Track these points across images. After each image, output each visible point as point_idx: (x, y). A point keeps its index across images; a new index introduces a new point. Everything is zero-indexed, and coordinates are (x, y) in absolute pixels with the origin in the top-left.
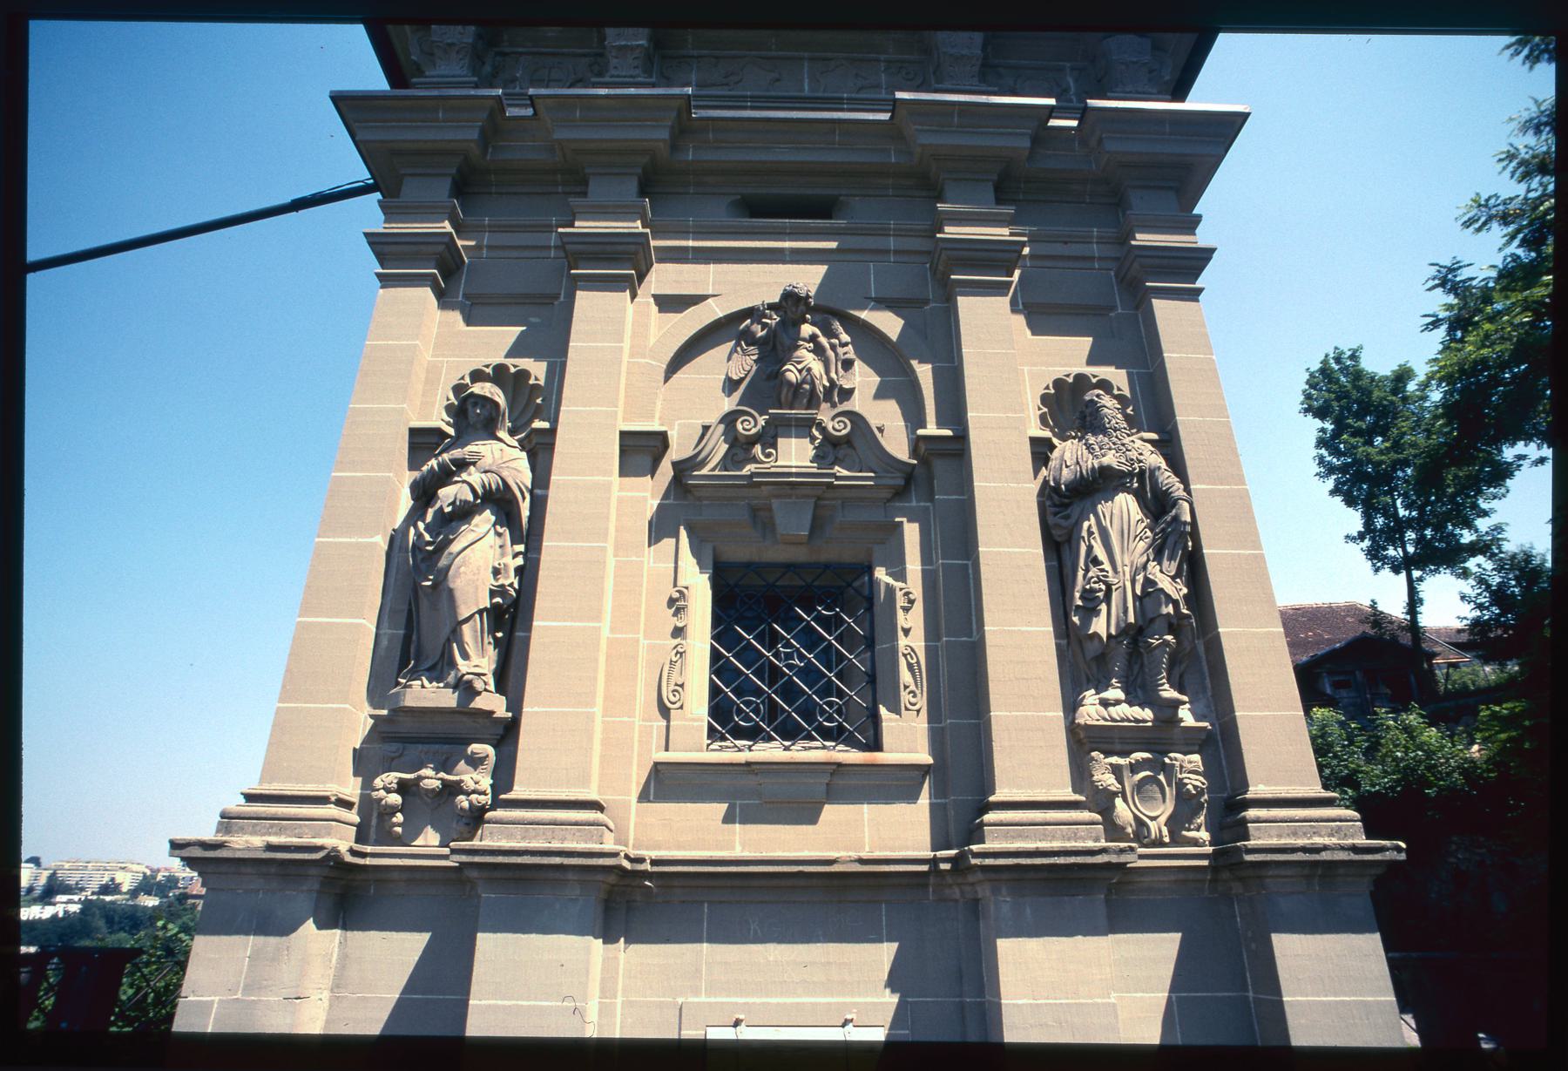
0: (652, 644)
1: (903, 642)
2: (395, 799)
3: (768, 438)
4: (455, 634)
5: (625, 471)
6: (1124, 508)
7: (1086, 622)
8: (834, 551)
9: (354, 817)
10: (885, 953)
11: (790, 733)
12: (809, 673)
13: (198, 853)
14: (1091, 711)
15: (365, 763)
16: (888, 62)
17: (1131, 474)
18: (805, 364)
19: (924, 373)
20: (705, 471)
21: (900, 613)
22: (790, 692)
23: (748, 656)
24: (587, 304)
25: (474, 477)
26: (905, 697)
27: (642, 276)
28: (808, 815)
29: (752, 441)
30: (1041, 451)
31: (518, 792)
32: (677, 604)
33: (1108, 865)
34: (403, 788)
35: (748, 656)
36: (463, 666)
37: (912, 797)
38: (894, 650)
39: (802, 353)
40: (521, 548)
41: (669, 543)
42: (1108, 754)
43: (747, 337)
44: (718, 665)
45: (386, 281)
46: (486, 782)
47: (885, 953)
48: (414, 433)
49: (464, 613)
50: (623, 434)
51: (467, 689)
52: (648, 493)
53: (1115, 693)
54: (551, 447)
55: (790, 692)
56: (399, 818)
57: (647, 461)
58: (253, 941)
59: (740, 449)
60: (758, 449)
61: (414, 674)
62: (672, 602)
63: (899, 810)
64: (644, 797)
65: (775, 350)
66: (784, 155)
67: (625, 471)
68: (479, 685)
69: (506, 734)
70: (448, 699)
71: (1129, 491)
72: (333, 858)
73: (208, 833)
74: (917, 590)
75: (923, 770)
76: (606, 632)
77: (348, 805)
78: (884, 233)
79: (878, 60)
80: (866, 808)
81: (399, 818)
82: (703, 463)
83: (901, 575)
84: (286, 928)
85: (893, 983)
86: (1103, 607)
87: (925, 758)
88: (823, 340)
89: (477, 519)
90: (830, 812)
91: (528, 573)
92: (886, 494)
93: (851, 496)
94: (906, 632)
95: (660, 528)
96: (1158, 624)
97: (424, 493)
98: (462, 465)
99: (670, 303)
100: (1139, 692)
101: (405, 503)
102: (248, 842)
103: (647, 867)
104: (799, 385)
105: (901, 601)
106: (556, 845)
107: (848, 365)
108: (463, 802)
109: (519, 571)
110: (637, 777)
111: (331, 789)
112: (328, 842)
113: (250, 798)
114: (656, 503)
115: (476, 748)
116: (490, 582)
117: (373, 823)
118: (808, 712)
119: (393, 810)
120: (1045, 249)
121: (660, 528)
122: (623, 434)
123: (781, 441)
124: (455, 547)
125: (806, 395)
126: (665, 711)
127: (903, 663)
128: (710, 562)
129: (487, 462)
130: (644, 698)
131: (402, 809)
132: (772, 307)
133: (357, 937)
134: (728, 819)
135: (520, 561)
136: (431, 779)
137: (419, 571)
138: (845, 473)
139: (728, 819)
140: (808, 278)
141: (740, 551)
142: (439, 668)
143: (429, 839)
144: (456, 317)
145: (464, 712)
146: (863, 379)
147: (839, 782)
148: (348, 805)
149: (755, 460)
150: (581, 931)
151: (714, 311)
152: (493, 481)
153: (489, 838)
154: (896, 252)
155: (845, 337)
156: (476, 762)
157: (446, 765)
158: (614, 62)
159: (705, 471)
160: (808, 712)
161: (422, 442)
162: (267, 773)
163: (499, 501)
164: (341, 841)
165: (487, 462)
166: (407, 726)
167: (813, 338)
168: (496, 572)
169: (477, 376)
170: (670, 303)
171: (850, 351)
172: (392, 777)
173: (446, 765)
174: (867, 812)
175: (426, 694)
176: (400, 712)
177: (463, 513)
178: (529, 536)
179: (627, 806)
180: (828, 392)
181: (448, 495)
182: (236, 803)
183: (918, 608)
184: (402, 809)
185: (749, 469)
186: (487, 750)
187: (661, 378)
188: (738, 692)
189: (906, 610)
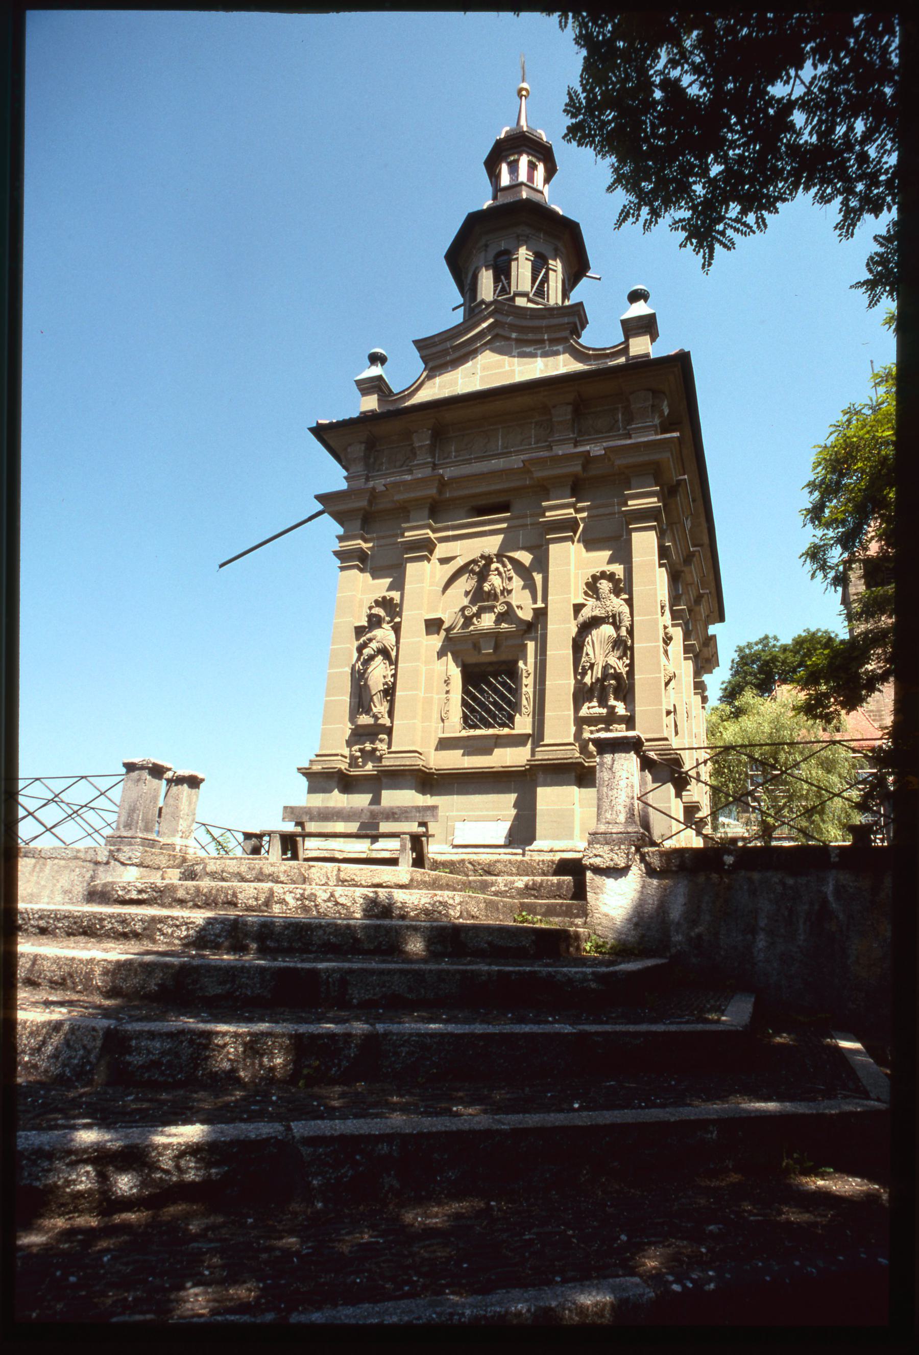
0: (438, 697)
1: (524, 689)
2: (358, 754)
3: (478, 615)
4: (372, 700)
5: (428, 633)
6: (607, 630)
7: (583, 677)
8: (504, 656)
9: (348, 760)
10: (513, 797)
11: (489, 725)
12: (495, 704)
13: (304, 771)
14: (584, 712)
15: (349, 744)
16: (536, 423)
17: (608, 617)
18: (495, 581)
19: (538, 578)
20: (455, 631)
21: (524, 679)
22: (489, 711)
23: (474, 698)
24: (411, 568)
25: (374, 645)
26: (524, 710)
27: (431, 552)
28: (489, 752)
29: (472, 617)
30: (578, 608)
31: (393, 749)
32: (447, 682)
33: (572, 763)
34: (361, 750)
35: (474, 698)
36: (375, 710)
37: (524, 745)
38: (521, 693)
39: (492, 577)
40: (393, 667)
41: (444, 658)
42: (589, 726)
43: (472, 572)
44: (464, 703)
45: (342, 569)
46: (385, 747)
47: (513, 797)
48: (356, 628)
49: (373, 692)
50: (426, 621)
51: (376, 717)
52: (437, 641)
53: (595, 703)
54: (400, 627)
55: (489, 711)
56: (360, 760)
57: (435, 628)
58: (321, 795)
59: (468, 621)
60: (475, 619)
61: (361, 714)
62: (445, 681)
63: (520, 749)
64: (436, 749)
65: (483, 576)
66: (483, 488)
67: (428, 633)
68: (380, 716)
69: (389, 731)
70: (371, 721)
71: (608, 623)
72: (340, 771)
73: (307, 766)
74: (531, 670)
75: (528, 736)
76: (422, 695)
77: (345, 757)
78: (525, 516)
79: (531, 423)
80: (508, 749)
81: (360, 760)
82: (454, 628)
83: (526, 664)
84: (330, 791)
85: (515, 806)
86: (589, 672)
87: (530, 731)
88: (501, 569)
89: (377, 659)
90: (497, 751)
91: (394, 676)
92: (521, 633)
93: (508, 635)
94: (526, 686)
95: (441, 654)
96: (609, 677)
97: (360, 649)
98: (370, 640)
99: (444, 561)
100: (603, 703)
101: (356, 655)
102: (317, 768)
103: (433, 771)
104: (489, 591)
105: (525, 674)
106: (403, 763)
107: (510, 579)
108: (378, 753)
109: (393, 676)
110: (434, 743)
111: (339, 751)
112: (339, 766)
113: (317, 756)
114: (440, 644)
115: (381, 736)
116: (383, 681)
117: (353, 762)
118: (494, 717)
119: (358, 758)
120: (595, 512)
121: (441, 654)
122: (426, 621)
123: (483, 615)
124: (369, 671)
125: (492, 596)
126: (443, 720)
127: (524, 698)
128: (460, 663)
129: (378, 638)
130: (436, 716)
131: (361, 757)
132: (366, 670)
133: (350, 796)
134: (463, 755)
135: (393, 672)
136: (368, 746)
137: (360, 680)
138: (506, 626)
139: (463, 755)
140: (491, 544)
141: (472, 659)
142: (368, 711)
143: (370, 766)
144: (368, 576)
145: (376, 725)
146: (517, 583)
147: (499, 741)
148: (345, 757)
149: (473, 624)
150: (411, 789)
151: (460, 562)
152: (380, 645)
153: (385, 762)
154: (531, 524)
155: (509, 567)
156: (381, 741)
157: (373, 742)
158: (418, 452)
159: (455, 631)
160: (494, 717)
161: (360, 631)
162: (321, 748)
163: (384, 652)
164: (343, 766)
165: (378, 638)
166: (361, 731)
167: (497, 569)
168: (384, 677)
169: (371, 608)
170: (444, 561)
171: (512, 573)
172: (357, 747)
173: (373, 742)
174: (509, 750)
175: (364, 720)
176: (358, 727)
177: (371, 658)
178: (394, 662)
179: (429, 752)
180: (502, 592)
181: (366, 651)
182: (314, 758)
183: (532, 676)
184: (361, 757)
185: (472, 628)
186: (385, 737)
187: (440, 593)
188: (471, 712)
189: (527, 677)
